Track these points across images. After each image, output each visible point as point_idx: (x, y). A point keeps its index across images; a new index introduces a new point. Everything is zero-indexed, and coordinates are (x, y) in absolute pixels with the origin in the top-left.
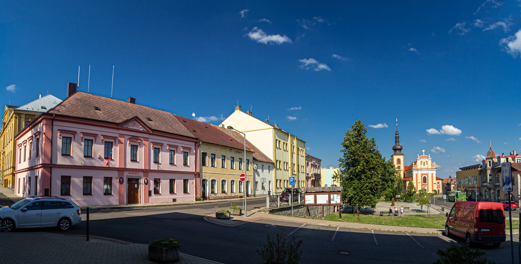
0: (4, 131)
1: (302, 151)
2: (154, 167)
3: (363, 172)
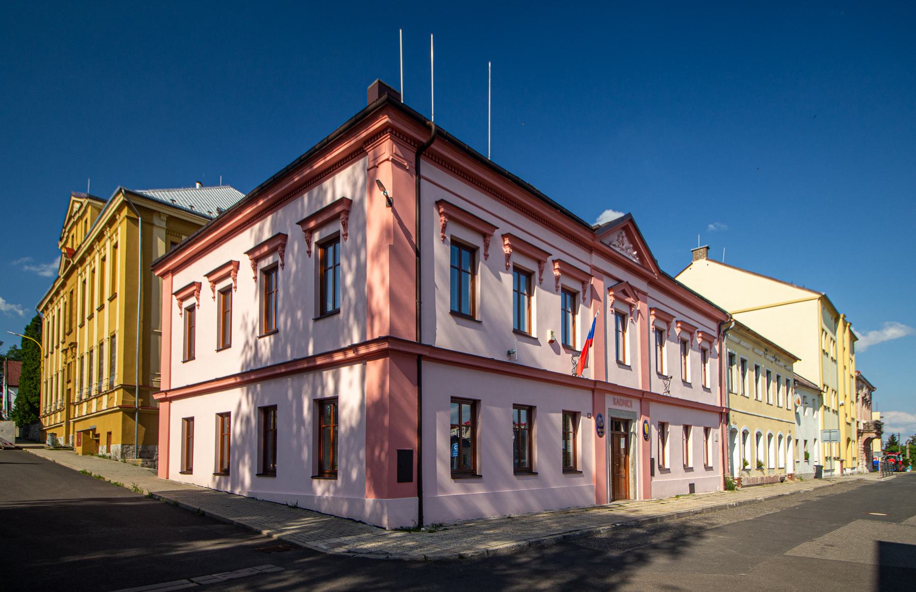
0: (67, 277)
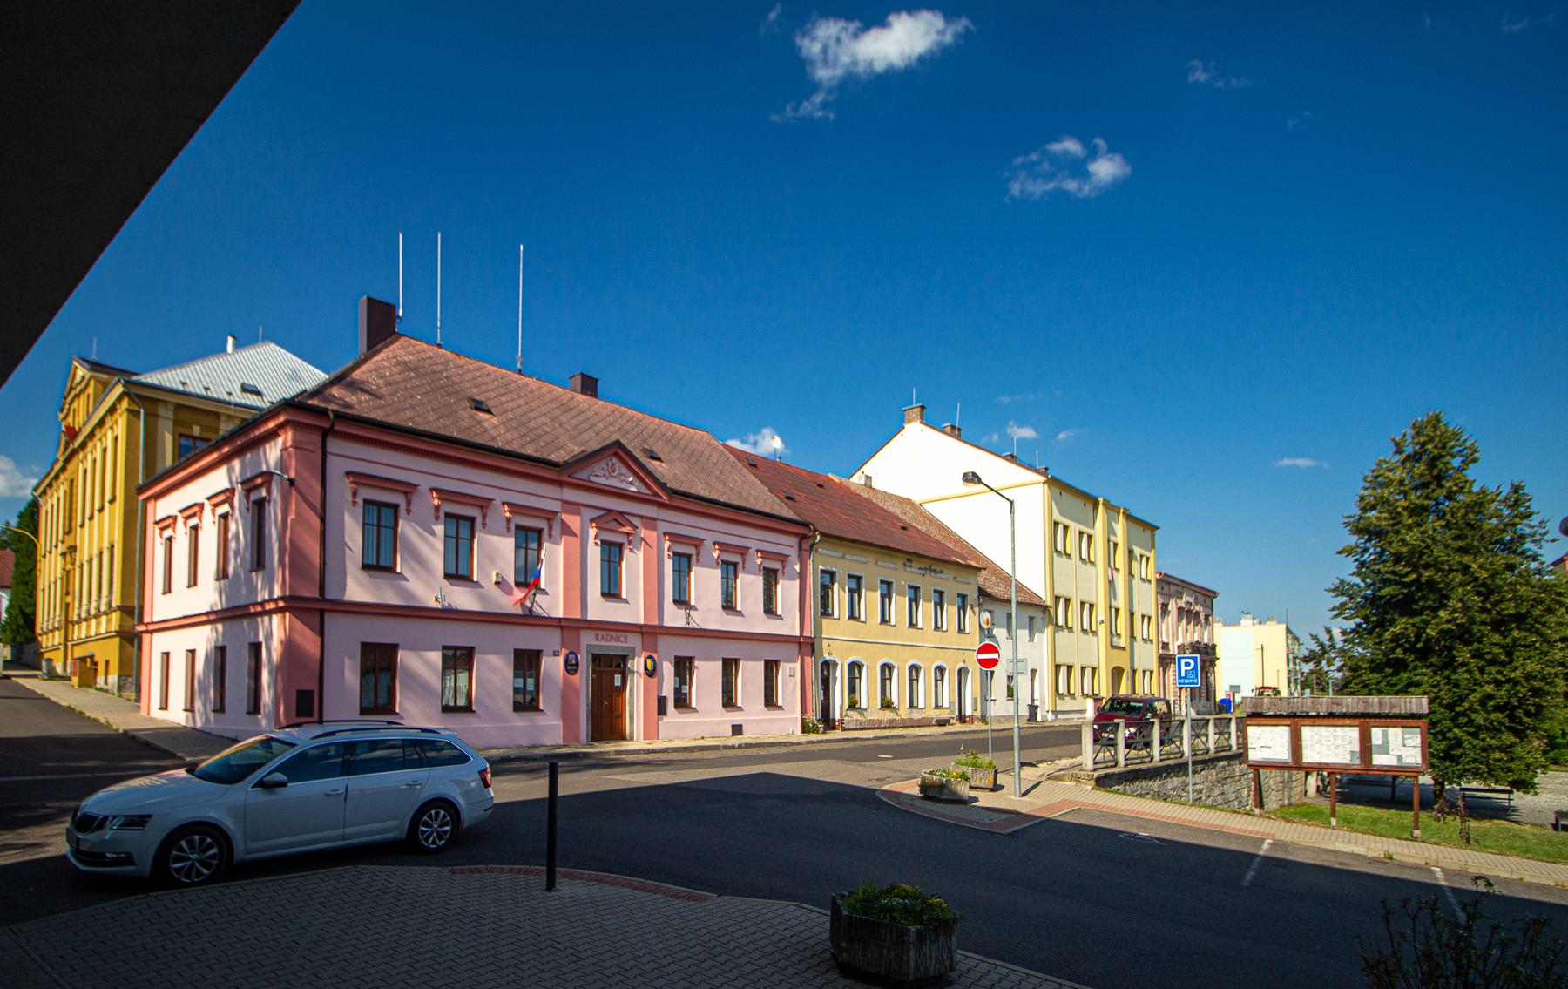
0: (68, 461)
1: (1144, 559)
2: (674, 617)
3: (1464, 634)
